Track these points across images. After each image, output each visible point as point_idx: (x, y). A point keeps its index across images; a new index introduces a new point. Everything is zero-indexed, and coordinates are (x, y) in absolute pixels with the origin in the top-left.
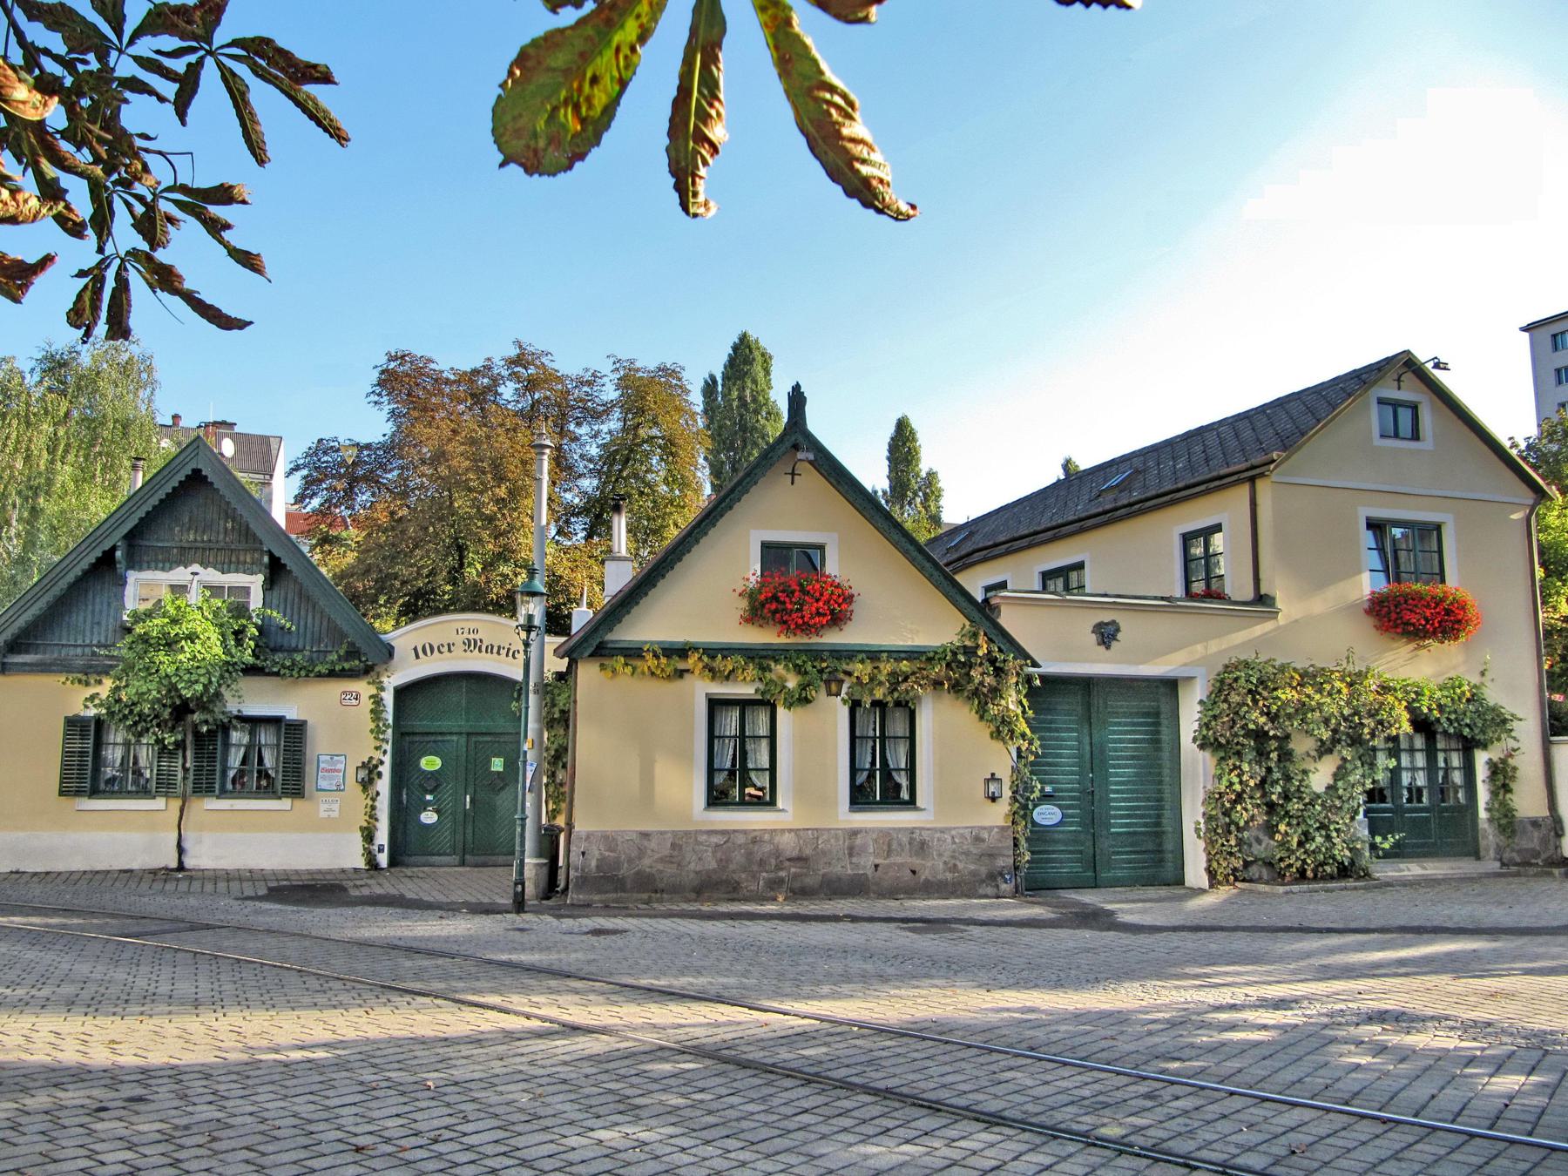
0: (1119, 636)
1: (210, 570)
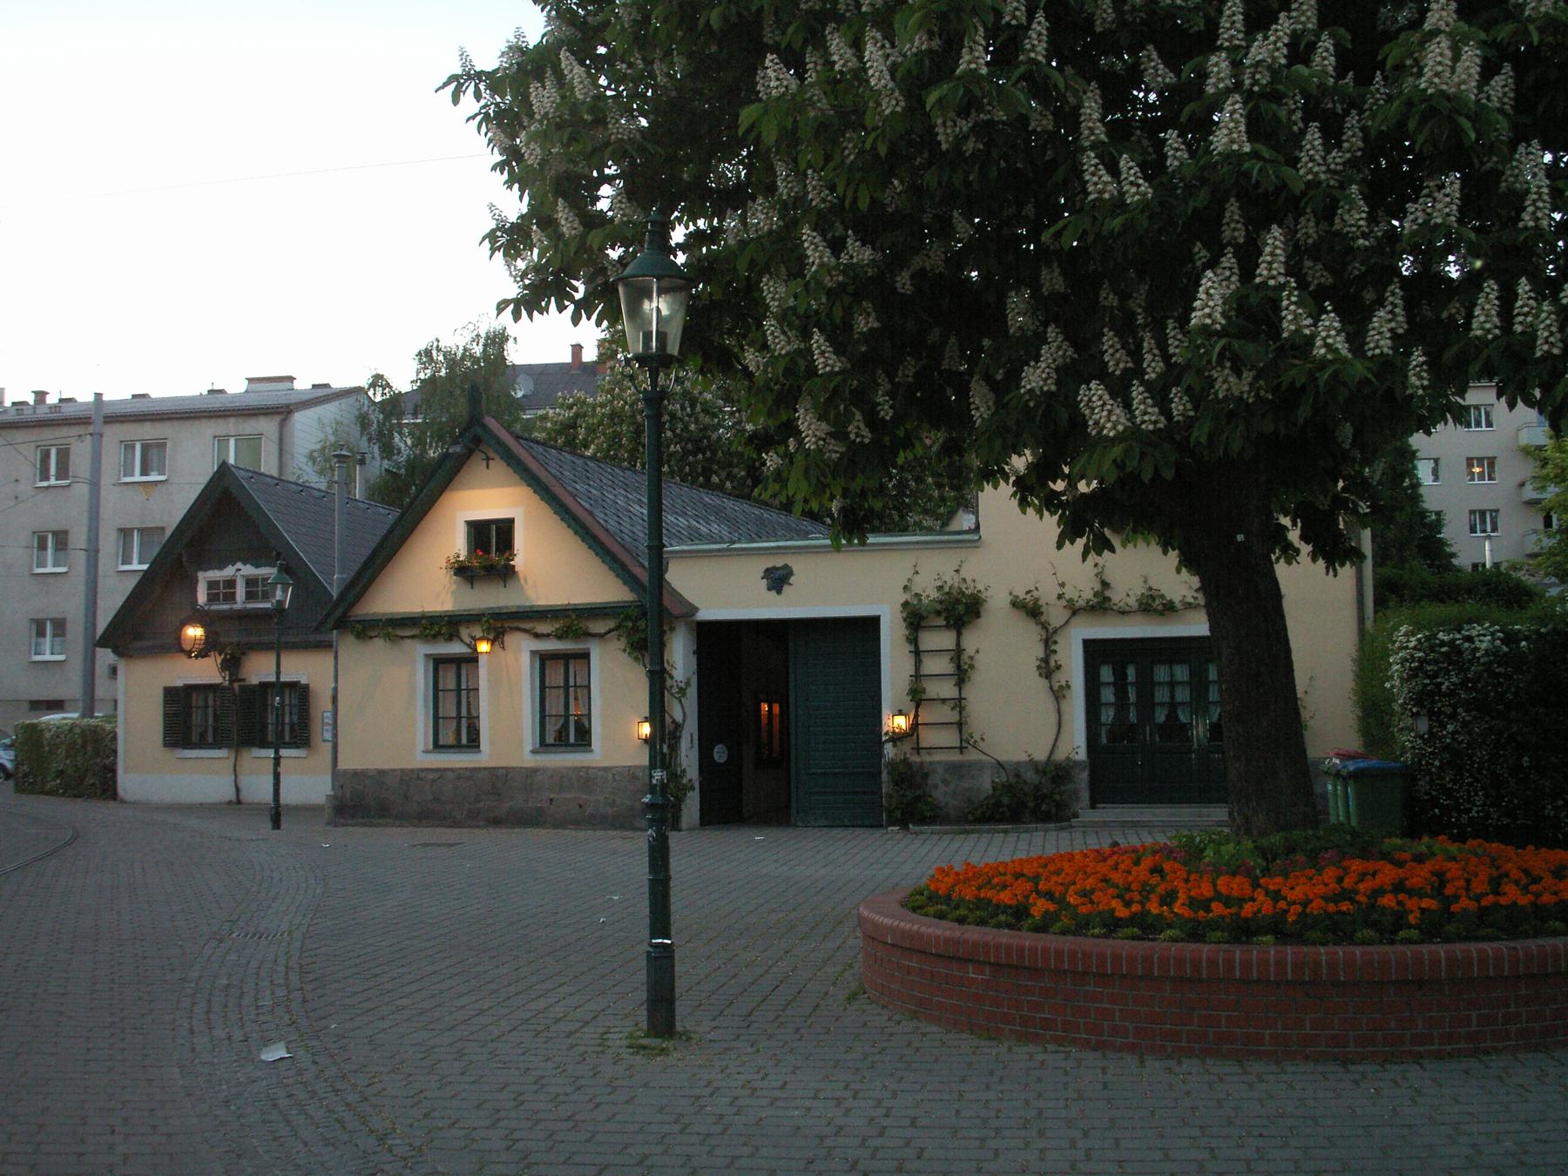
0: (792, 580)
1: (248, 566)
